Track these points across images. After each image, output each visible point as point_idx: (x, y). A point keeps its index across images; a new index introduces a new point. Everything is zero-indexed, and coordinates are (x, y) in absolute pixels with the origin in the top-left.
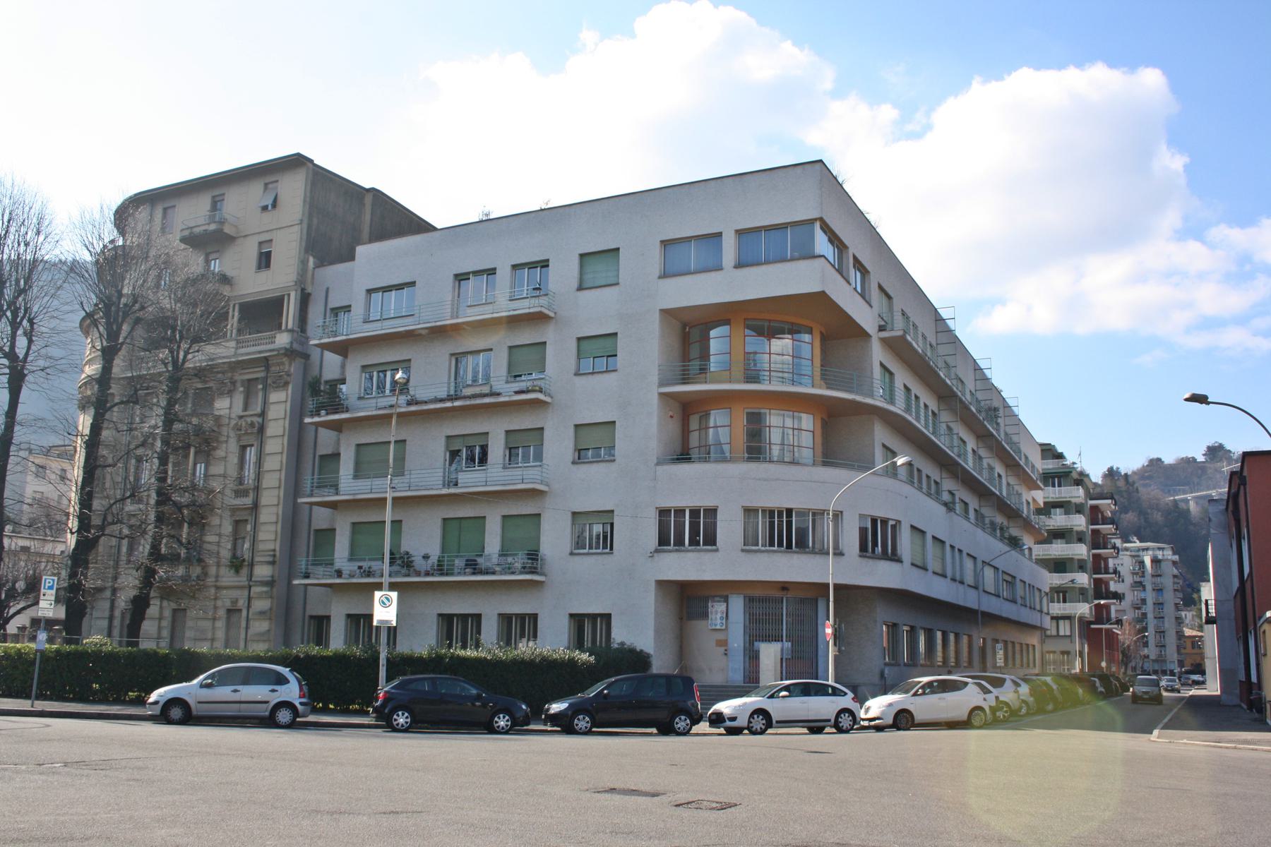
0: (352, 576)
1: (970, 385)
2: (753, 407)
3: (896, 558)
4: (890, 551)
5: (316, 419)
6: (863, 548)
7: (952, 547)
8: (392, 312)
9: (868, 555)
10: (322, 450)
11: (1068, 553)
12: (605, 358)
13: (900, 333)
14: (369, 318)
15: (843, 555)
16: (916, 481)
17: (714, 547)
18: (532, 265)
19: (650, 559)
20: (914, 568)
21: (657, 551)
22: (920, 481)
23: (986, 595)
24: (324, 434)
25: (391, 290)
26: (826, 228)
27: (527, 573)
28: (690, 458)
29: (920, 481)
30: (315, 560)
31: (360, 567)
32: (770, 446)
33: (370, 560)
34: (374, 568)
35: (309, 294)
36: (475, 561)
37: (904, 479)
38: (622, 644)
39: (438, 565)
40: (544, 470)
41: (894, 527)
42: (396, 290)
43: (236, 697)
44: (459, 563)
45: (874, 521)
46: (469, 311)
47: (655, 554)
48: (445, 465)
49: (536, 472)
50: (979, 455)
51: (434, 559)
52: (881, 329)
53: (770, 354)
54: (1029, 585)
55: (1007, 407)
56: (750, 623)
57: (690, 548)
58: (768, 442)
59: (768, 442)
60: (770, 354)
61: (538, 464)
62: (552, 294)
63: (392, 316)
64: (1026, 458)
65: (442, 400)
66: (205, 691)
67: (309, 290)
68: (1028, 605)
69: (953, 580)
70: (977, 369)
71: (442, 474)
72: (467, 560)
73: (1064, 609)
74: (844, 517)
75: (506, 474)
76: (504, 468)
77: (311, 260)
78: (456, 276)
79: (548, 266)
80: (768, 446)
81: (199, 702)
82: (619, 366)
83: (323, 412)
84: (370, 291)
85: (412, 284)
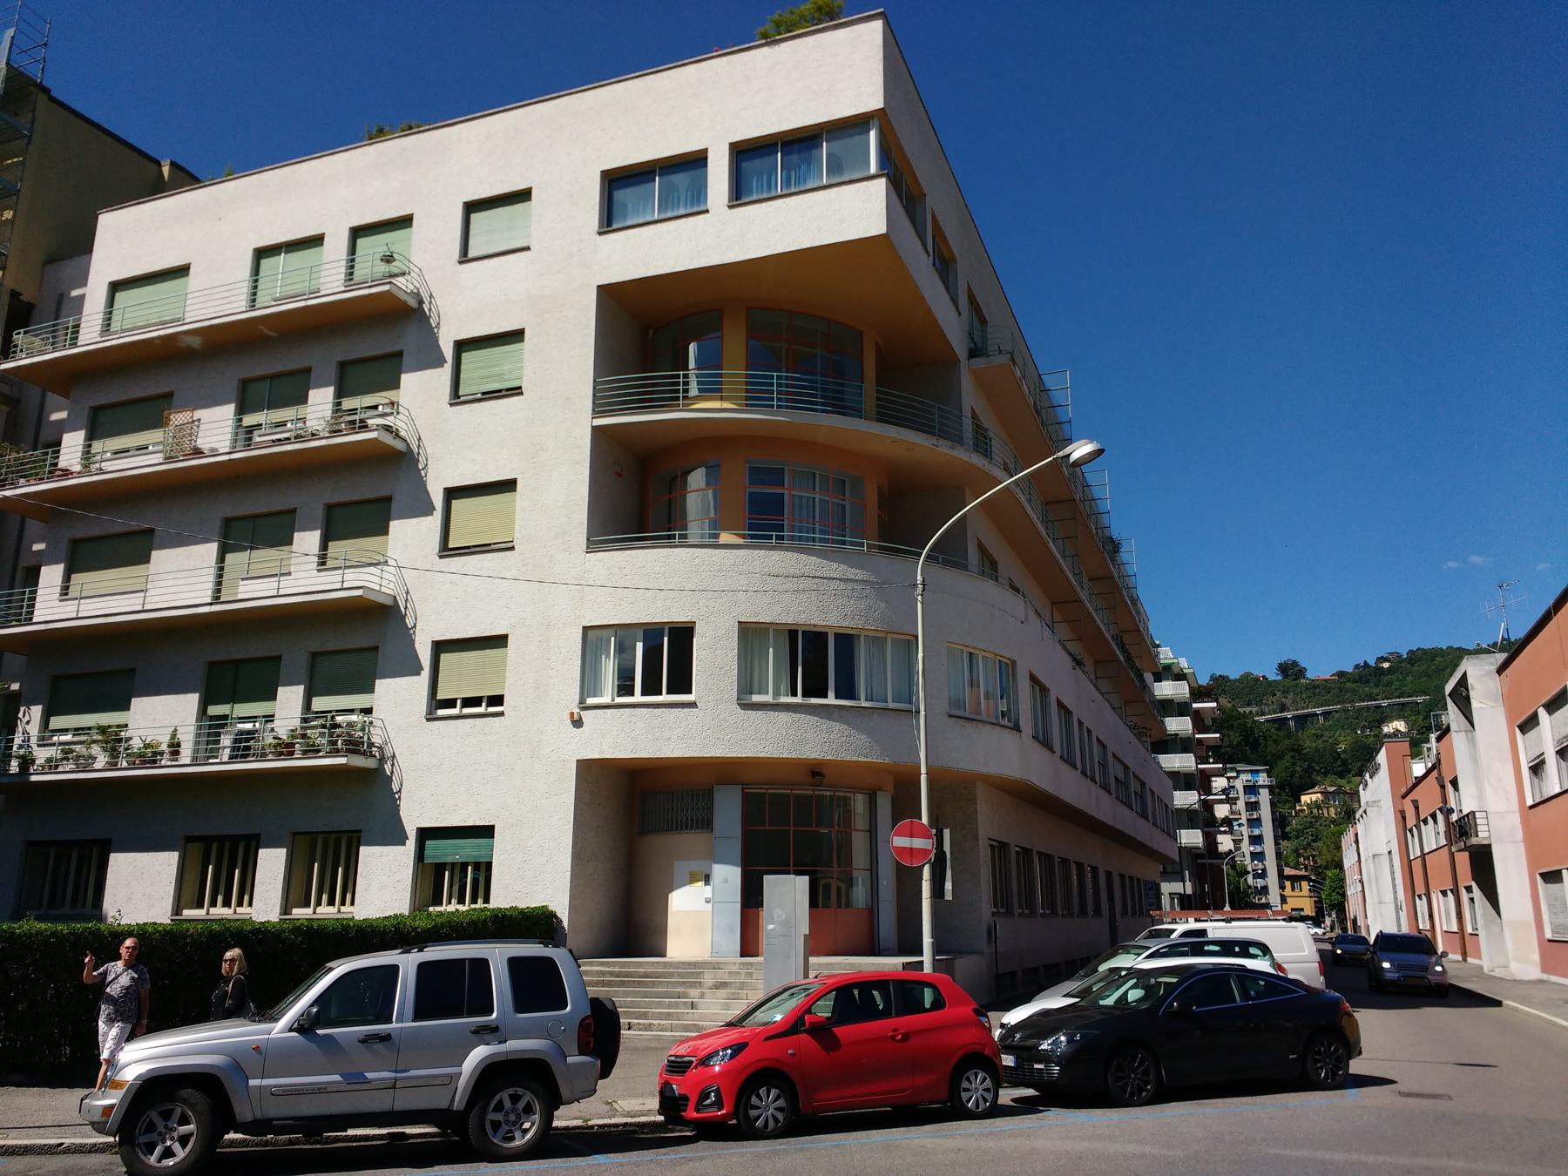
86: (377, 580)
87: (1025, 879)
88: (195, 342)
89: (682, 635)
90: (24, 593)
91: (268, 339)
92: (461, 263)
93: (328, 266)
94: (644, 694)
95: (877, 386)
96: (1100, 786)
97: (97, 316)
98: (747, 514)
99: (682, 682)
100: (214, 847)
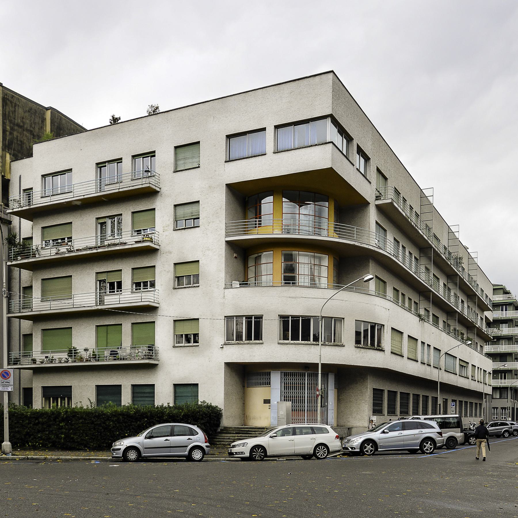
0: (42, 363)
1: (444, 242)
2: (288, 251)
3: (380, 348)
4: (376, 344)
5: (14, 263)
6: (358, 342)
7: (423, 343)
8: (59, 189)
9: (361, 346)
10: (24, 284)
11: (509, 350)
12: (193, 220)
13: (390, 201)
14: (45, 194)
15: (344, 346)
16: (400, 301)
17: (261, 341)
18: (144, 155)
19: (221, 349)
20: (393, 356)
21: (225, 344)
22: (404, 302)
23: (447, 373)
24: (25, 274)
25: (58, 175)
26: (335, 122)
27: (146, 359)
28: (247, 284)
29: (404, 302)
30: (25, 353)
31: (47, 357)
32: (298, 276)
33: (52, 352)
34: (55, 357)
35: (9, 180)
36: (117, 352)
37: (374, 293)
38: (204, 402)
39: (93, 355)
40: (155, 293)
41: (380, 330)
42: (61, 175)
43: (167, 444)
44: (107, 353)
45: (373, 327)
46: (106, 187)
47: (224, 346)
48: (96, 290)
49: (151, 295)
50: (448, 288)
51: (90, 352)
52: (378, 198)
53: (299, 214)
54: (478, 368)
55: (470, 258)
56: (284, 389)
57: (246, 342)
58: (297, 274)
59: (297, 274)
60: (299, 214)
61: (153, 289)
62: (158, 175)
63: (59, 192)
64: (482, 291)
65: (90, 248)
66: (148, 440)
67: (7, 177)
68: (477, 380)
69: (423, 363)
70: (450, 232)
71: (94, 296)
72: (111, 351)
73: (505, 383)
74: (345, 322)
75: (133, 295)
76: (132, 292)
77: (8, 156)
78: (97, 164)
79: (154, 156)
80: (297, 275)
81: (145, 448)
82: (200, 224)
83: (19, 258)
84: (43, 176)
85: (70, 170)
86: (153, 295)
87: (307, 400)
88: (79, 203)
89: (259, 319)
90: (256, 221)
91: (104, 201)
92: (174, 172)
93: (125, 175)
94: (254, 340)
95: (334, 222)
96: (459, 375)
97: (39, 193)
98: (283, 273)
99: (258, 336)
100: (135, 399)
